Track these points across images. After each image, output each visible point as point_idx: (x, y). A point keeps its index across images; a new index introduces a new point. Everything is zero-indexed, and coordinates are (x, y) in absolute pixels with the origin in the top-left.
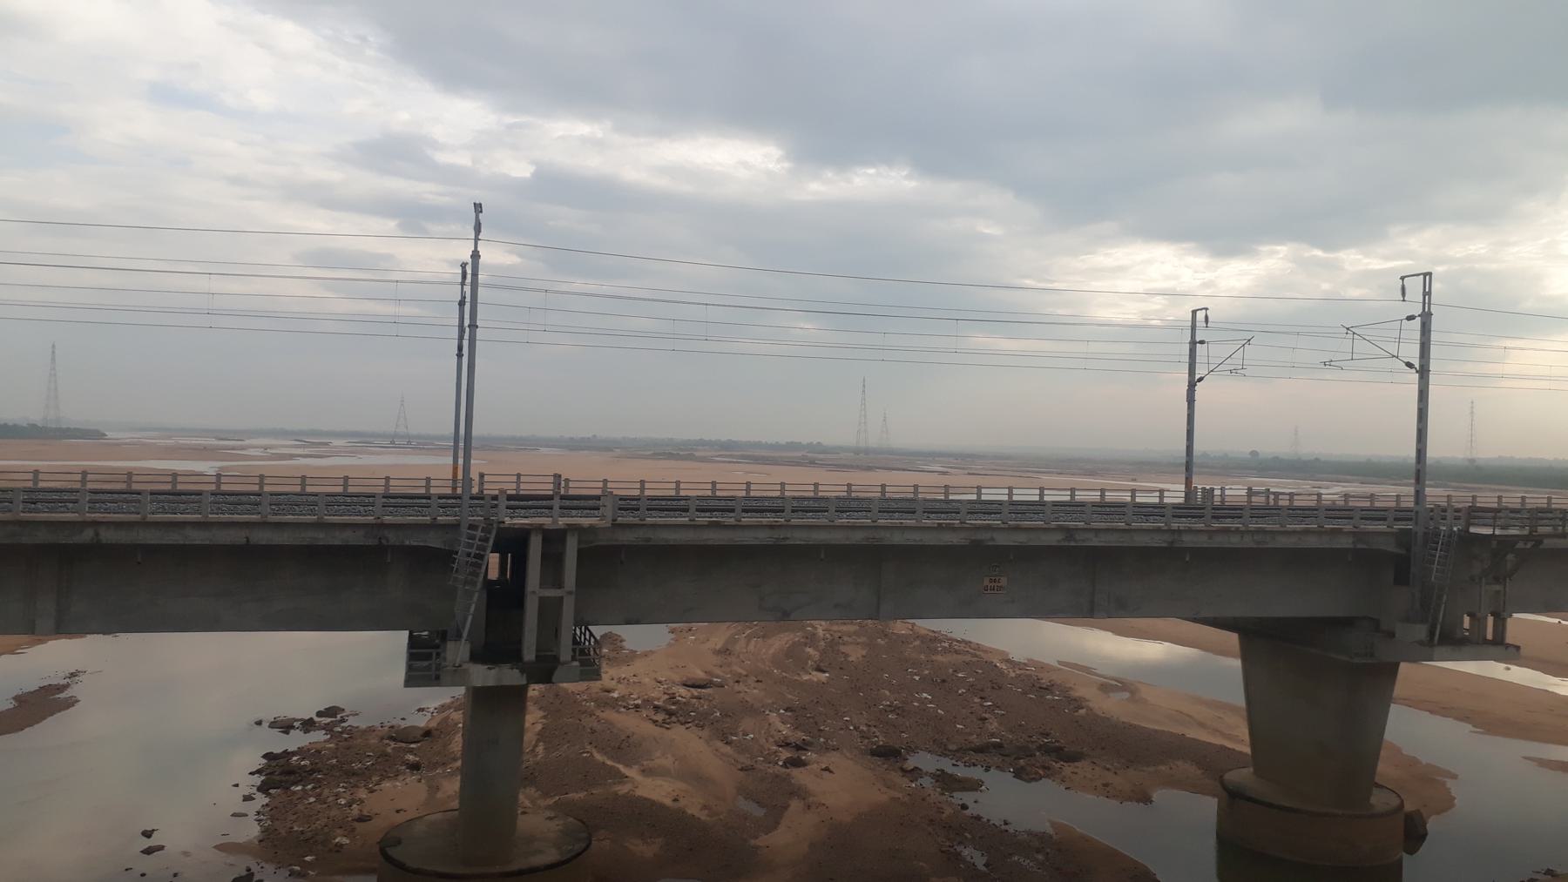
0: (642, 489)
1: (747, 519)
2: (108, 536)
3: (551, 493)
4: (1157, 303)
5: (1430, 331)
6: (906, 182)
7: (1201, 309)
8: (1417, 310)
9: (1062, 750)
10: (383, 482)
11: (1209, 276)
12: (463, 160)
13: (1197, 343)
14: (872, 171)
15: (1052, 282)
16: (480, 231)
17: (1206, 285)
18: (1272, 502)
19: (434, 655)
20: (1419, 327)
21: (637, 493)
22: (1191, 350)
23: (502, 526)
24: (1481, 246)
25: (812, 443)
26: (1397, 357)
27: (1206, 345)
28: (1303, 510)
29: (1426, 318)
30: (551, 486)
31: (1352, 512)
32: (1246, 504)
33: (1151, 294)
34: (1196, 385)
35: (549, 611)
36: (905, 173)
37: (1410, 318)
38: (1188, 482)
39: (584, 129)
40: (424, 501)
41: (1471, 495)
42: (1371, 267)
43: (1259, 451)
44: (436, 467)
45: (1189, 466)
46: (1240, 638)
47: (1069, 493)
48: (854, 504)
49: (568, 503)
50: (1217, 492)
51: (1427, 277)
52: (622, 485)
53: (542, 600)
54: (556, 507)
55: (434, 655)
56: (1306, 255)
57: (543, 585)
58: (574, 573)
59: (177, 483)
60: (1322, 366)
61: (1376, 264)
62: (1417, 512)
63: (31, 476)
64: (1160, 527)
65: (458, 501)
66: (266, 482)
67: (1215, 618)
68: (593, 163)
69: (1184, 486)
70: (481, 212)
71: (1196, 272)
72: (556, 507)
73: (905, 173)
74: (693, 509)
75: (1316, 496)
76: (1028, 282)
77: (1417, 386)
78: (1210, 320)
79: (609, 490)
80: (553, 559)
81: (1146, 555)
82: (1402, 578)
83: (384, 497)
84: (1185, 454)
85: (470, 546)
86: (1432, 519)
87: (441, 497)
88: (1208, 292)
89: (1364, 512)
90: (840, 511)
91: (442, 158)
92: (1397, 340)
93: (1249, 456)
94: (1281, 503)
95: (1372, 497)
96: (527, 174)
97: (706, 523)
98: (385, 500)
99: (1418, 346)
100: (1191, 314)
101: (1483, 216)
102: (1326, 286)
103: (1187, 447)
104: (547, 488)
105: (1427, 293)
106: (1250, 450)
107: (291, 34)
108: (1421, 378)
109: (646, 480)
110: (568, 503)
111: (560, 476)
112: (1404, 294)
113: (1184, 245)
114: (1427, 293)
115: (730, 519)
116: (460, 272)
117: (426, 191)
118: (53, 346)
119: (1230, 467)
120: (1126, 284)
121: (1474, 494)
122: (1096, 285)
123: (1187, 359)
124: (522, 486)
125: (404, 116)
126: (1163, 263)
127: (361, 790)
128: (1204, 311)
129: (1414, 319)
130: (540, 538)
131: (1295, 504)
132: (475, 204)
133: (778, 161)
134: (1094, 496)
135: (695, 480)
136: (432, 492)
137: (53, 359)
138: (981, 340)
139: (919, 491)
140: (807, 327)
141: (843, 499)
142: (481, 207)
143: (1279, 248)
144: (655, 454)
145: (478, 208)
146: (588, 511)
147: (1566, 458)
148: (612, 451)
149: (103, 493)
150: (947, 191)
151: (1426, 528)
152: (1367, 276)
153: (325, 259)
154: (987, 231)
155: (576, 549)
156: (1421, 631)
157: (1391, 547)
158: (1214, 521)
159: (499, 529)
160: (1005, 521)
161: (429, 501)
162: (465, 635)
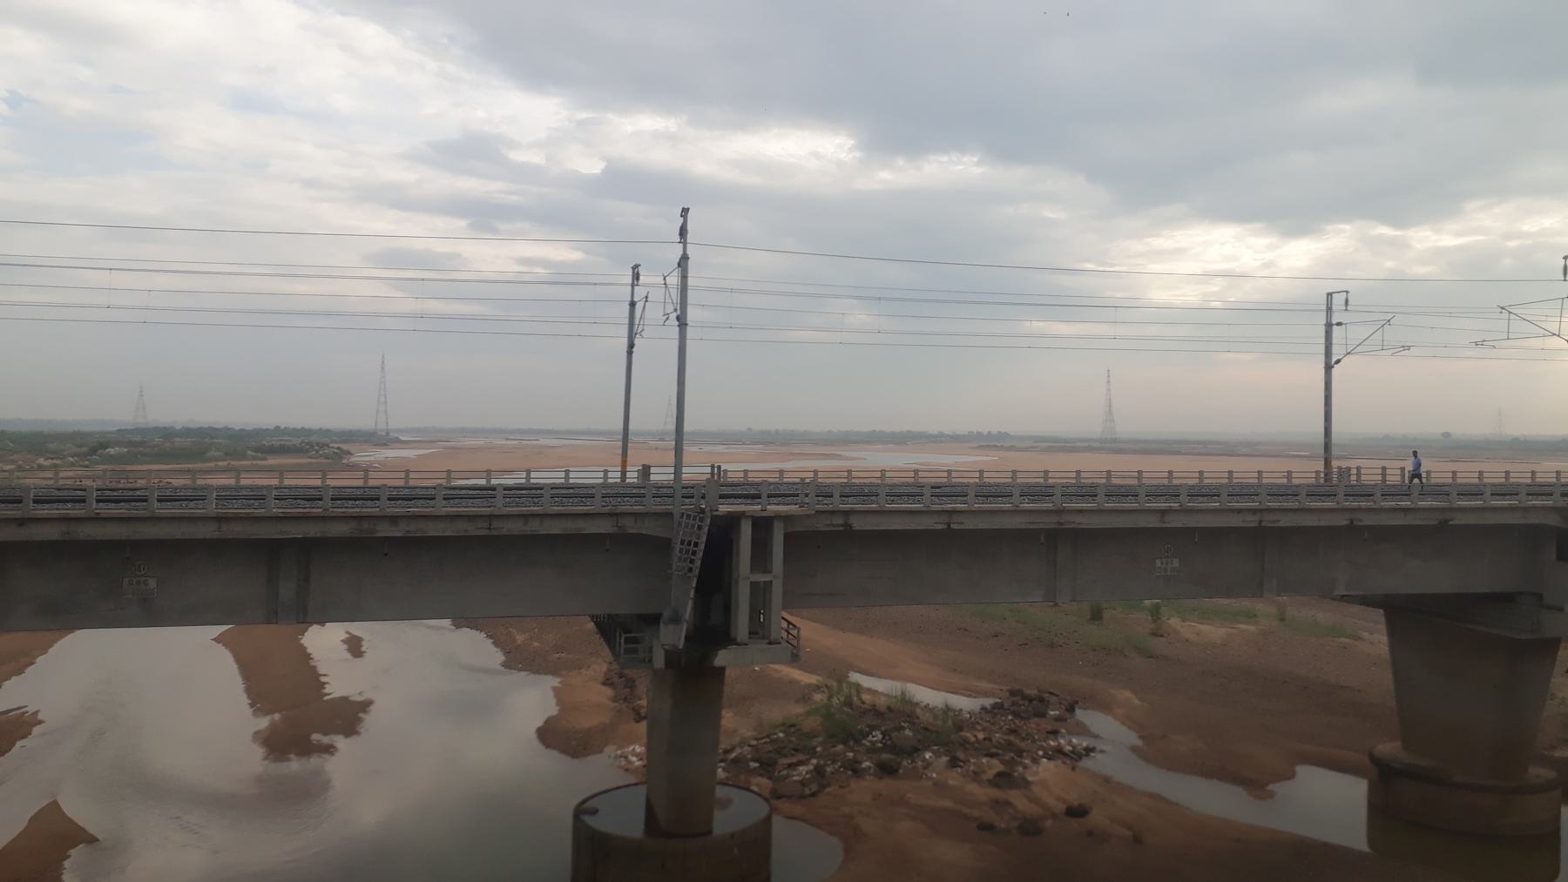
1: (45, 511)
2: (858, 524)
4: (1215, 287)
12: (535, 158)
13: (1333, 325)
14: (945, 158)
23: (715, 513)
25: (874, 431)
26: (1558, 336)
27: (1344, 326)
33: (1209, 276)
34: (1333, 367)
35: (760, 594)
36: (975, 159)
38: (1327, 463)
39: (648, 122)
40: (490, 492)
44: (1307, 471)
45: (1327, 446)
50: (1354, 471)
53: (754, 585)
57: (752, 570)
59: (1233, 478)
61: (1448, 240)
63: (977, 475)
68: (660, 157)
73: (975, 159)
75: (846, 473)
78: (1349, 303)
84: (1323, 436)
86: (703, 497)
88: (1266, 273)
91: (517, 156)
100: (1325, 296)
102: (1390, 264)
107: (371, 35)
109: (1432, 470)
111: (1404, 468)
112: (1565, 274)
116: (631, 274)
118: (1108, 371)
123: (1323, 340)
126: (1222, 244)
127: (749, 756)
130: (750, 523)
133: (850, 150)
135: (1216, 469)
140: (860, 317)
141: (1072, 486)
144: (980, 447)
146: (353, 502)
150: (1013, 176)
153: (394, 258)
154: (1051, 216)
159: (714, 518)
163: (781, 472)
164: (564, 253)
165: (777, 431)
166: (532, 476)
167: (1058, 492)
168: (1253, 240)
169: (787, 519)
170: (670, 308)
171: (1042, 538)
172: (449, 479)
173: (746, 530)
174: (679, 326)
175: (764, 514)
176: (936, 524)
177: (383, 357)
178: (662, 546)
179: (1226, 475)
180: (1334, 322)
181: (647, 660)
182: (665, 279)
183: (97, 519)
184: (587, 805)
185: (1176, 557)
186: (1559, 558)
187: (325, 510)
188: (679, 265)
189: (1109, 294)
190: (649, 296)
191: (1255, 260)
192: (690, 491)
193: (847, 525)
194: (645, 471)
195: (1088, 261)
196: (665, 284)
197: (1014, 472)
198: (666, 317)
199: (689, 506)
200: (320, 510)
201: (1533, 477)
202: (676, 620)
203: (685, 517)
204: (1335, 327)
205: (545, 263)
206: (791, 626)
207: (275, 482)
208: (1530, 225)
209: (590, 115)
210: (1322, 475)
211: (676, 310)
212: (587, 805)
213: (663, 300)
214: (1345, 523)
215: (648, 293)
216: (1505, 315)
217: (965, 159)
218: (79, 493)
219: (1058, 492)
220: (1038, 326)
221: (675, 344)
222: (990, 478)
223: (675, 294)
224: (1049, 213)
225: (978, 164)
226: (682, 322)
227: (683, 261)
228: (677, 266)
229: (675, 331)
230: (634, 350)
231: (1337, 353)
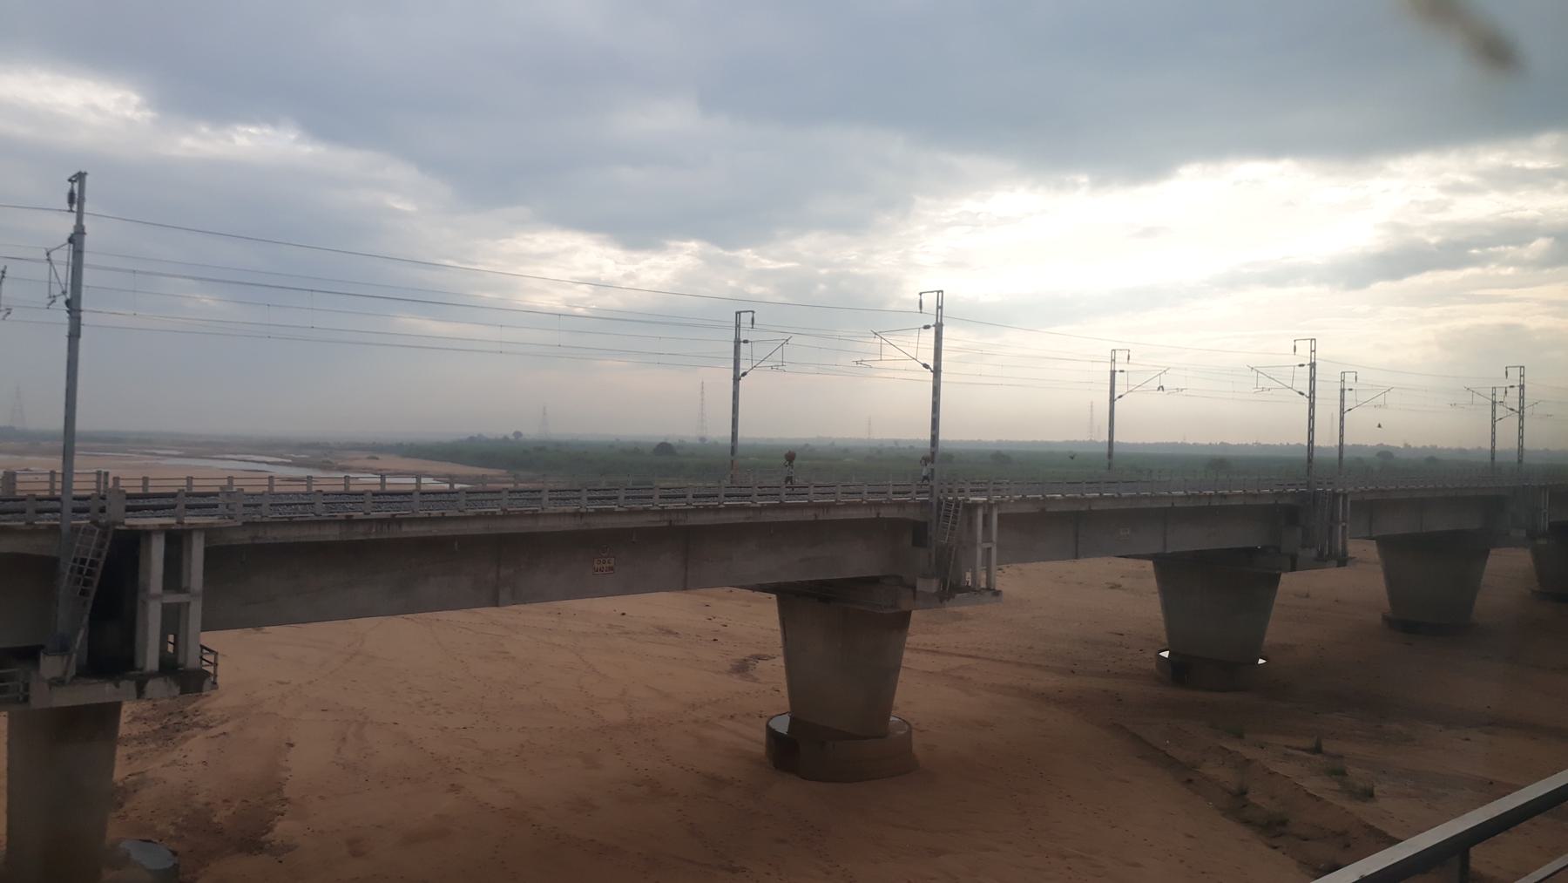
8: (932, 322)
10: (140, 483)
11: (631, 268)
14: (253, 130)
15: (476, 264)
17: (629, 276)
27: (750, 344)
30: (47, 486)
31: (834, 489)
32: (94, 492)
41: (343, 475)
51: (940, 294)
53: (166, 609)
57: (983, 542)
61: (768, 264)
62: (932, 487)
64: (1038, 498)
65: (57, 505)
74: (968, 490)
76: (448, 262)
77: (931, 384)
79: (121, 489)
80: (986, 518)
87: (130, 497)
88: (631, 283)
92: (916, 345)
93: (513, 437)
99: (933, 351)
100: (734, 314)
101: (851, 226)
102: (732, 283)
103: (733, 433)
105: (940, 307)
106: (514, 430)
109: (150, 477)
112: (1295, 351)
114: (940, 307)
118: (703, 383)
119: (114, 442)
120: (550, 271)
123: (1109, 382)
132: (86, 174)
133: (138, 108)
139: (194, 484)
140: (207, 302)
149: (429, 493)
150: (347, 160)
152: (761, 276)
154: (399, 206)
156: (933, 586)
160: (366, 511)
161: (590, 495)
166: (141, 489)
169: (208, 531)
170: (57, 291)
173: (157, 549)
174: (80, 311)
175: (180, 527)
178: (47, 566)
180: (742, 339)
181: (21, 698)
182: (48, 254)
187: (27, 524)
188: (71, 240)
190: (8, 271)
192: (82, 505)
193: (1043, 510)
196: (49, 260)
198: (52, 299)
200: (23, 523)
201: (145, 486)
202: (63, 649)
204: (742, 344)
206: (205, 651)
210: (59, 478)
211: (64, 293)
213: (48, 279)
214: (813, 518)
215: (6, 267)
216: (878, 340)
223: (64, 273)
225: (138, 108)
226: (73, 306)
227: (76, 239)
228: (66, 241)
229: (63, 316)
231: (744, 367)
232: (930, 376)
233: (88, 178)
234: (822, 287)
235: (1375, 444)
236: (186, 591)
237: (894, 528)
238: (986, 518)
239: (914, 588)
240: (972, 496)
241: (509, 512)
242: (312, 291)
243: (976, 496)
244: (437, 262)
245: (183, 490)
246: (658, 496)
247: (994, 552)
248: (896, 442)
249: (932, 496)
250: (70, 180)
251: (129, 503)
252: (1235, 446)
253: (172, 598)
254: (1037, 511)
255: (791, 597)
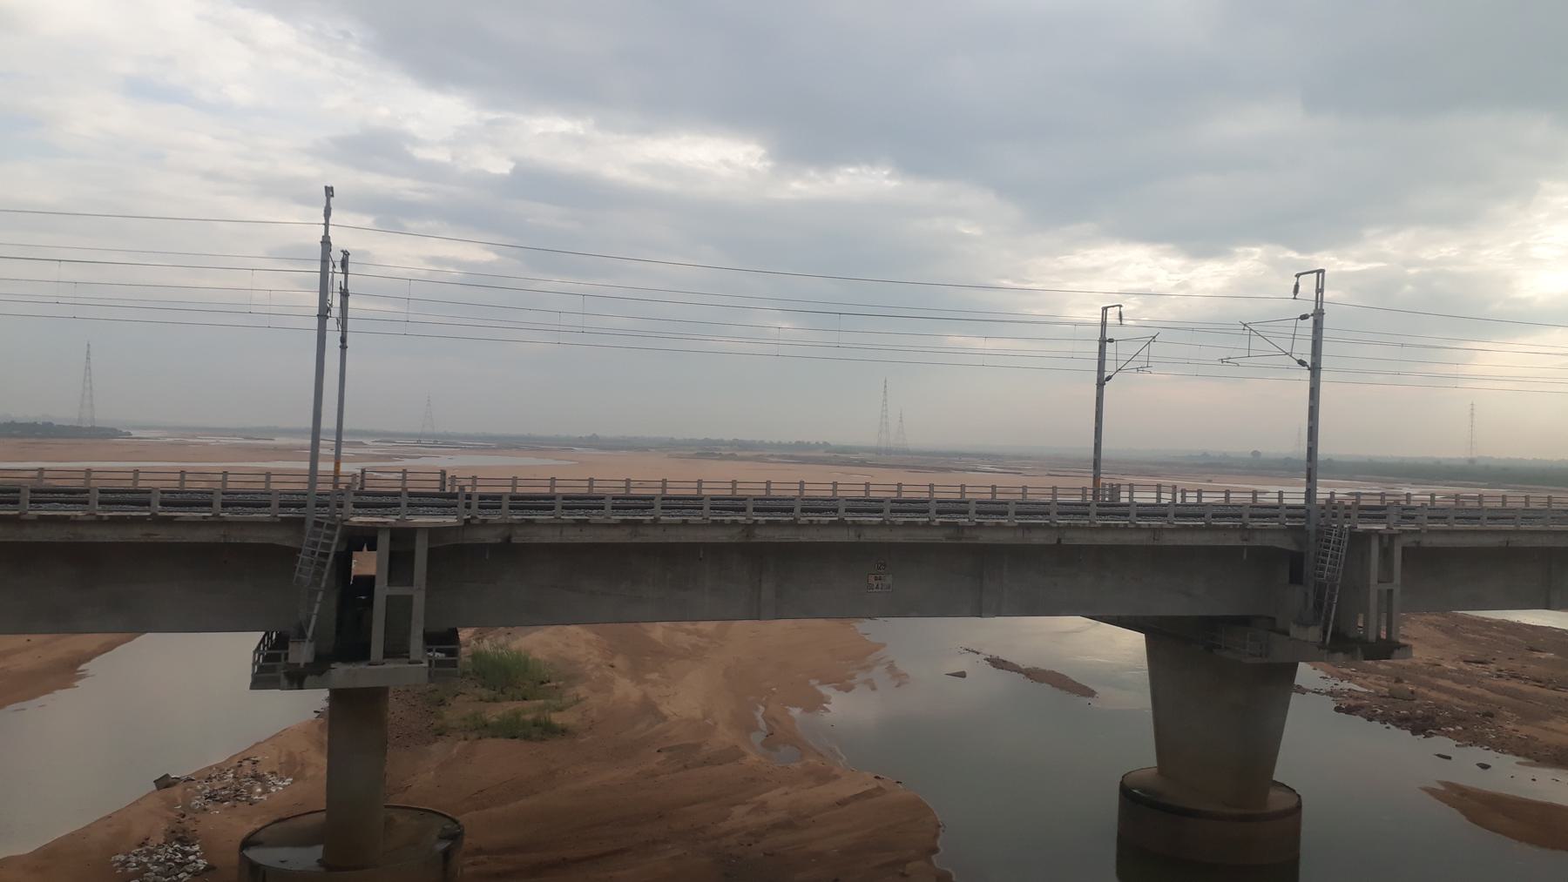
0: (931, 492)
3: (400, 490)
5: (1322, 329)
6: (886, 182)
7: (1113, 306)
9: (1474, 742)
11: (1183, 277)
12: (441, 156)
14: (851, 170)
16: (330, 214)
17: (1180, 286)
18: (1179, 501)
19: (283, 657)
20: (1311, 325)
21: (926, 495)
22: (1100, 347)
23: (346, 523)
24: (1452, 249)
26: (1291, 356)
28: (685, 499)
29: (1319, 315)
30: (437, 484)
31: (603, 501)
36: (886, 173)
37: (1304, 317)
38: (1096, 478)
39: (563, 125)
42: (1344, 269)
43: (1259, 450)
44: (1075, 487)
45: (1097, 463)
46: (1146, 637)
47: (1196, 494)
48: (1032, 508)
49: (415, 500)
52: (749, 486)
54: (404, 505)
55: (283, 657)
56: (1281, 256)
58: (424, 570)
60: (1220, 363)
62: (1308, 511)
63: (624, 484)
66: (738, 487)
67: (1119, 617)
68: (572, 160)
69: (308, 463)
70: (333, 196)
71: (1171, 273)
72: (404, 505)
76: (1006, 283)
80: (1386, 553)
81: (1019, 556)
82: (1296, 577)
83: (223, 494)
85: (315, 544)
86: (1323, 517)
89: (166, 496)
90: (225, 505)
91: (421, 154)
94: (1189, 500)
95: (1457, 497)
96: (507, 171)
97: (994, 525)
98: (225, 497)
101: (1457, 220)
103: (1096, 444)
104: (434, 487)
106: (1252, 450)
107: (271, 29)
108: (1313, 375)
109: (1412, 493)
110: (415, 500)
113: (1161, 247)
114: (1320, 291)
115: (595, 517)
117: (403, 187)
121: (1527, 494)
122: (1072, 285)
124: (1155, 495)
125: (384, 111)
126: (1138, 264)
128: (1118, 308)
129: (1308, 318)
131: (518, 491)
132: (326, 187)
133: (761, 160)
134: (1218, 498)
135: (718, 477)
136: (92, 485)
137: (88, 358)
138: (957, 340)
142: (332, 191)
143: (1254, 249)
145: (329, 191)
147: (1566, 458)
148: (647, 450)
150: (928, 191)
151: (1317, 525)
154: (967, 232)
155: (426, 549)
157: (1285, 543)
158: (565, 512)
162: (309, 634)
163: (268, 475)
164: (476, 254)
165: (808, 443)
167: (973, 508)
168: (1168, 261)
169: (434, 532)
171: (702, 553)
172: (514, 486)
176: (938, 536)
177: (88, 345)
179: (220, 477)
183: (100, 521)
184: (251, 839)
185: (889, 574)
186: (1291, 582)
189: (1026, 311)
191: (1169, 280)
194: (1115, 490)
195: (1006, 277)
197: (700, 482)
199: (324, 513)
200: (701, 518)
202: (301, 635)
203: (318, 529)
205: (457, 263)
207: (509, 490)
208: (1428, 254)
209: (499, 116)
210: (1090, 492)
212: (251, 839)
217: (874, 173)
218: (301, 497)
219: (608, 503)
220: (956, 340)
221: (1306, 386)
222: (811, 491)
224: (966, 228)
225: (889, 177)
230: (340, 344)
231: (1109, 368)
232: (1307, 374)
233: (1326, 273)
234: (1409, 288)
235: (1531, 458)
236: (411, 584)
237: (1264, 558)
238: (1386, 553)
239: (1287, 633)
240: (354, 514)
241: (1058, 524)
242: (60, 261)
243: (667, 520)
244: (995, 282)
245: (1426, 504)
246: (1173, 514)
247: (1397, 592)
248: (1205, 454)
249: (1308, 522)
250: (1296, 276)
251: (1361, 512)
252: (703, 440)
253: (1388, 586)
254: (499, 540)
255: (1158, 632)
